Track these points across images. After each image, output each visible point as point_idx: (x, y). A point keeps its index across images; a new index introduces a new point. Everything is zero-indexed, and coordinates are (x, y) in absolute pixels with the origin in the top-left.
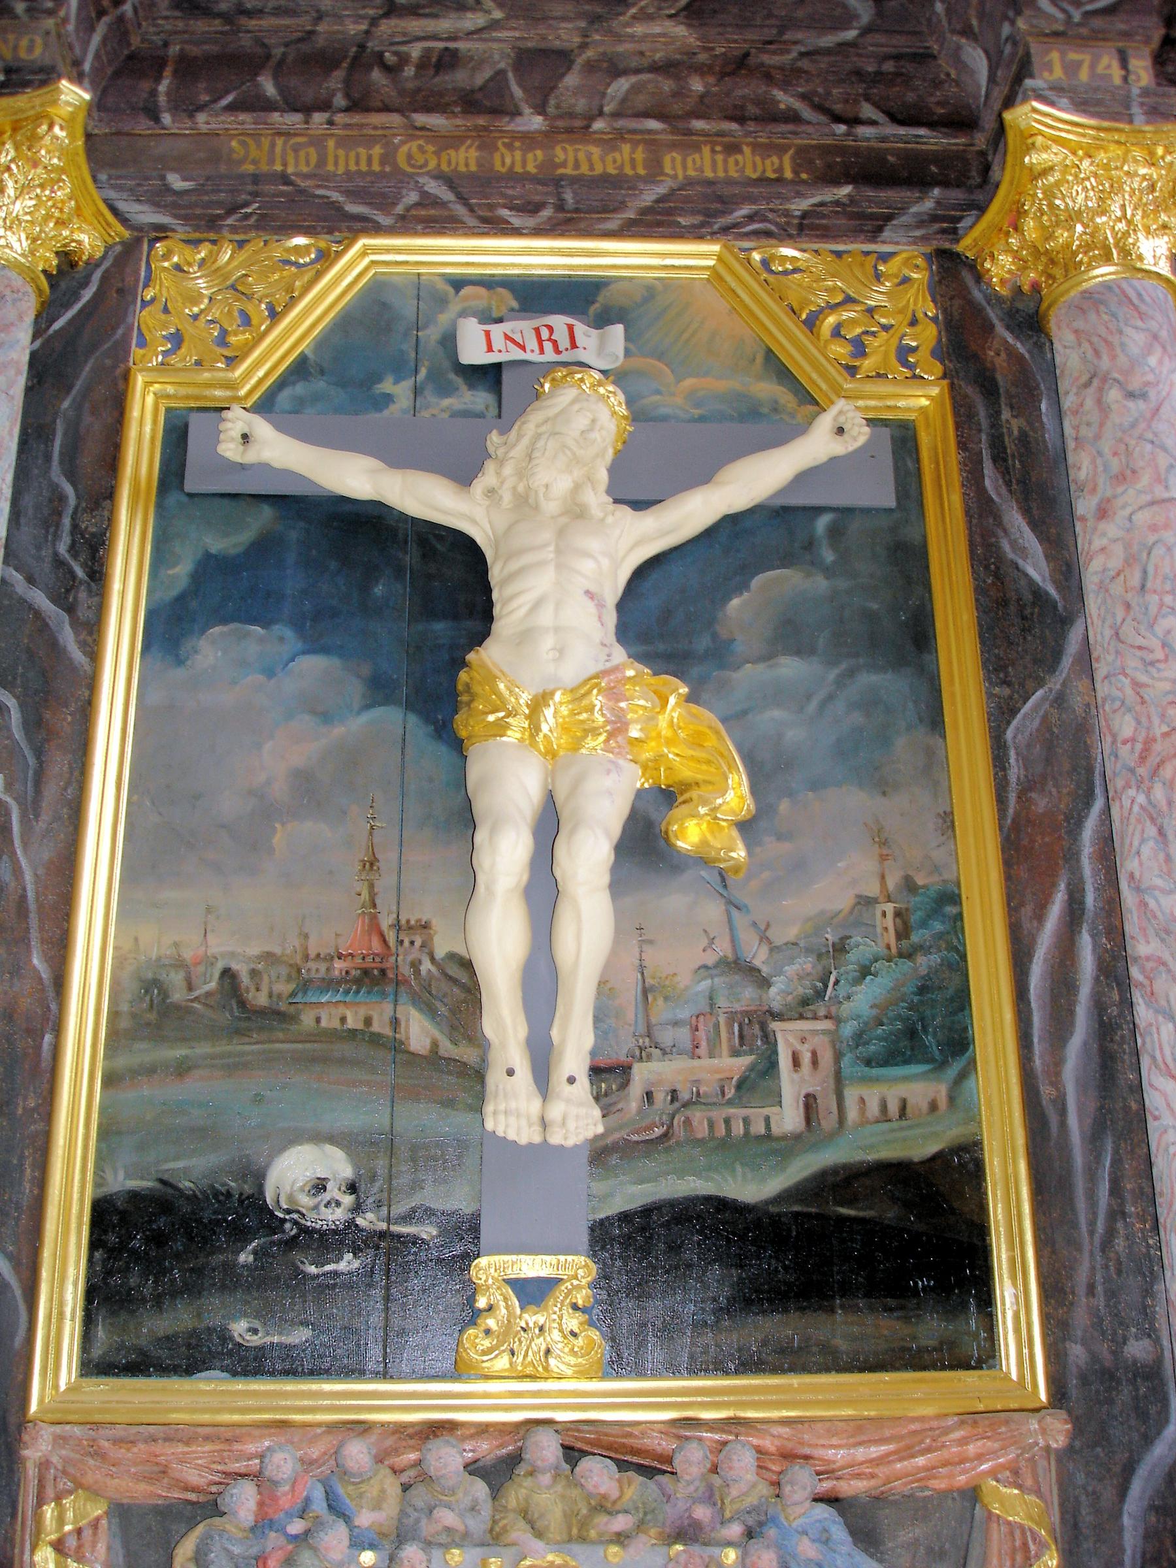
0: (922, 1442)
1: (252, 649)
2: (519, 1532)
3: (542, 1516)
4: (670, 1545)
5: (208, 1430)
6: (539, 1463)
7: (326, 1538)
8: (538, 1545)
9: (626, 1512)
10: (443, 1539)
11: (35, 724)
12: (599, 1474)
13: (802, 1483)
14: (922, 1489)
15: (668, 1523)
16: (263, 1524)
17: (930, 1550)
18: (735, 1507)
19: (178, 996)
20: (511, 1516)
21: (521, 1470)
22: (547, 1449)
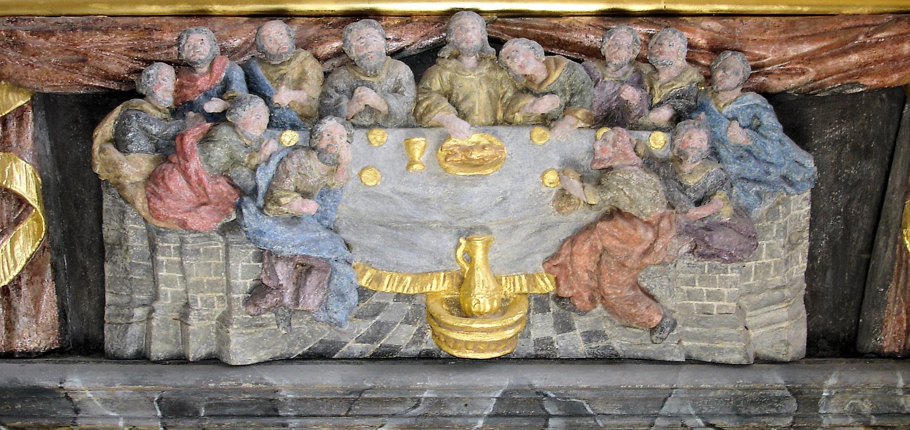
0: (856, 38)
2: (444, 114)
3: (466, 98)
4: (598, 128)
5: (129, 20)
6: (464, 45)
7: (244, 114)
8: (464, 125)
9: (552, 93)
10: (366, 120)
12: (525, 56)
13: (732, 71)
14: (853, 85)
15: (596, 105)
16: (182, 107)
17: (855, 148)
18: (665, 91)
20: (435, 97)
21: (445, 53)
22: (473, 33)
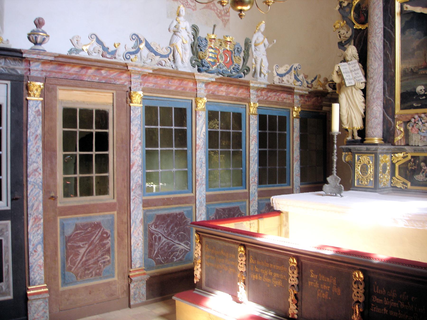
1: (412, 32)
11: (390, 45)
16: (415, 122)
19: (407, 72)
